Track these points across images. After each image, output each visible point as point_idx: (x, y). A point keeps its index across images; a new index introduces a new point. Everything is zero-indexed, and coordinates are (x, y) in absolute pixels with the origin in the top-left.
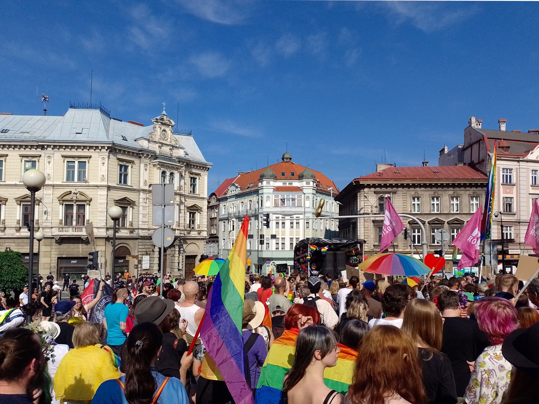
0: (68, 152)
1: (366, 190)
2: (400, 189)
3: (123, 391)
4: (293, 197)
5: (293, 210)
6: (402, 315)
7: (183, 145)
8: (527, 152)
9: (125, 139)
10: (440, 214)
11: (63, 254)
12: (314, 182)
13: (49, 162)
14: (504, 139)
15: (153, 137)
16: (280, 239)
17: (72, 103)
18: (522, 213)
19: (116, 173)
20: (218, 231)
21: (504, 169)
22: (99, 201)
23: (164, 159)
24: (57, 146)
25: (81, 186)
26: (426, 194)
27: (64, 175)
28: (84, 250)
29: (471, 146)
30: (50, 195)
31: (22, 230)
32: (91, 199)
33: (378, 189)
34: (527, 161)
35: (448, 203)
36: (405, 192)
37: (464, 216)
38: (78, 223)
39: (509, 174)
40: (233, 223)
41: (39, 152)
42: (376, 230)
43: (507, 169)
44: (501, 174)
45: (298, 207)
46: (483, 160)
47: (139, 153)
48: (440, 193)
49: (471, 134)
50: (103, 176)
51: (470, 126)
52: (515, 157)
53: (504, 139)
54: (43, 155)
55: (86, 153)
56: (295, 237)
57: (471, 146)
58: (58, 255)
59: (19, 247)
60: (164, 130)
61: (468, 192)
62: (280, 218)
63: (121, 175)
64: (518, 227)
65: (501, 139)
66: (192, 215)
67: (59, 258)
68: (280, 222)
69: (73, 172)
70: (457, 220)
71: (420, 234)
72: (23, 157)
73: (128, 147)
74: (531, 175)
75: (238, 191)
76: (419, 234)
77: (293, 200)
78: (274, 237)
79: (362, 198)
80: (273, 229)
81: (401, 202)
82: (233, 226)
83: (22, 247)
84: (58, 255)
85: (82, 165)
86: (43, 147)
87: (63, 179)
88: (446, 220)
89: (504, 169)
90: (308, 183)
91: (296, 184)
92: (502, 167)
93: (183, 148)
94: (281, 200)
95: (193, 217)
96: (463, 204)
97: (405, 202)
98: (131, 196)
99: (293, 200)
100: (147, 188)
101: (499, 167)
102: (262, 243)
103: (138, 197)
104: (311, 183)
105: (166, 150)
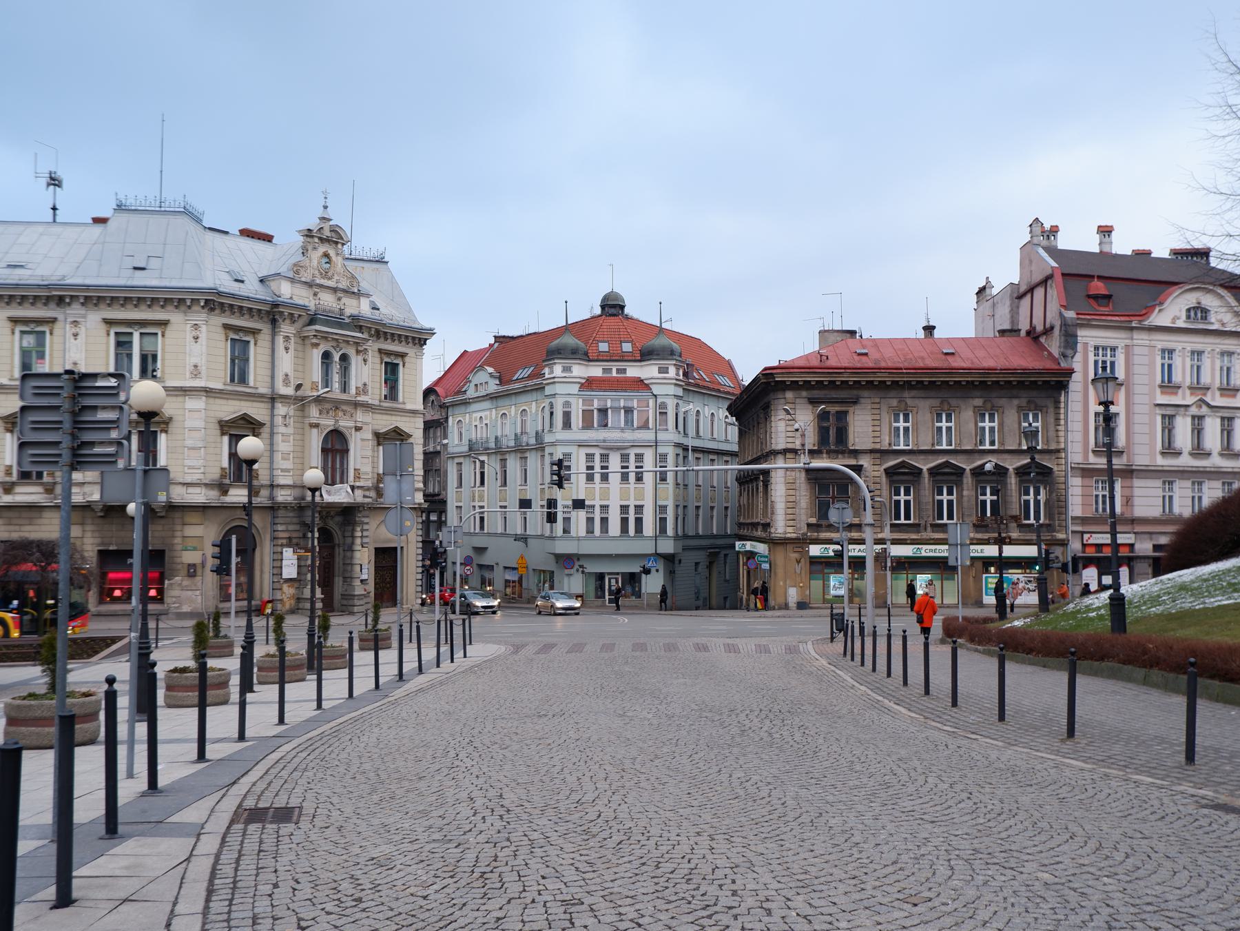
1: (789, 395)
2: (865, 393)
4: (629, 404)
5: (629, 436)
8: (1149, 310)
10: (911, 452)
11: (110, 544)
12: (677, 367)
13: (75, 335)
14: (1099, 277)
16: (597, 509)
18: (1137, 449)
19: (222, 360)
20: (444, 486)
21: (1096, 348)
22: (188, 424)
23: (327, 323)
26: (923, 408)
29: (1031, 290)
31: (232, 492)
32: (171, 419)
33: (816, 394)
35: (972, 426)
36: (877, 400)
37: (1006, 456)
39: (1108, 359)
42: (812, 489)
43: (1104, 348)
44: (1092, 358)
45: (639, 428)
47: (273, 313)
49: (1031, 261)
50: (196, 366)
52: (1123, 319)
53: (1099, 277)
54: (60, 317)
56: (632, 503)
57: (1031, 290)
58: (99, 545)
59: (12, 528)
61: (1016, 402)
62: (597, 458)
64: (1127, 483)
65: (1093, 277)
67: (102, 553)
68: (597, 469)
69: (130, 356)
71: (911, 498)
73: (248, 299)
74: (1159, 361)
75: (493, 386)
76: (907, 498)
77: (629, 411)
78: (579, 504)
79: (782, 415)
80: (578, 486)
82: (482, 474)
83: (17, 528)
84: (99, 545)
86: (60, 301)
87: (12, 371)
88: (925, 465)
89: (1096, 348)
90: (663, 370)
91: (633, 371)
92: (1092, 343)
93: (368, 296)
94: (599, 410)
96: (1006, 429)
97: (877, 423)
98: (258, 411)
99: (629, 411)
100: (289, 391)
102: (551, 518)
103: (269, 412)
104: (672, 371)
105: (328, 301)
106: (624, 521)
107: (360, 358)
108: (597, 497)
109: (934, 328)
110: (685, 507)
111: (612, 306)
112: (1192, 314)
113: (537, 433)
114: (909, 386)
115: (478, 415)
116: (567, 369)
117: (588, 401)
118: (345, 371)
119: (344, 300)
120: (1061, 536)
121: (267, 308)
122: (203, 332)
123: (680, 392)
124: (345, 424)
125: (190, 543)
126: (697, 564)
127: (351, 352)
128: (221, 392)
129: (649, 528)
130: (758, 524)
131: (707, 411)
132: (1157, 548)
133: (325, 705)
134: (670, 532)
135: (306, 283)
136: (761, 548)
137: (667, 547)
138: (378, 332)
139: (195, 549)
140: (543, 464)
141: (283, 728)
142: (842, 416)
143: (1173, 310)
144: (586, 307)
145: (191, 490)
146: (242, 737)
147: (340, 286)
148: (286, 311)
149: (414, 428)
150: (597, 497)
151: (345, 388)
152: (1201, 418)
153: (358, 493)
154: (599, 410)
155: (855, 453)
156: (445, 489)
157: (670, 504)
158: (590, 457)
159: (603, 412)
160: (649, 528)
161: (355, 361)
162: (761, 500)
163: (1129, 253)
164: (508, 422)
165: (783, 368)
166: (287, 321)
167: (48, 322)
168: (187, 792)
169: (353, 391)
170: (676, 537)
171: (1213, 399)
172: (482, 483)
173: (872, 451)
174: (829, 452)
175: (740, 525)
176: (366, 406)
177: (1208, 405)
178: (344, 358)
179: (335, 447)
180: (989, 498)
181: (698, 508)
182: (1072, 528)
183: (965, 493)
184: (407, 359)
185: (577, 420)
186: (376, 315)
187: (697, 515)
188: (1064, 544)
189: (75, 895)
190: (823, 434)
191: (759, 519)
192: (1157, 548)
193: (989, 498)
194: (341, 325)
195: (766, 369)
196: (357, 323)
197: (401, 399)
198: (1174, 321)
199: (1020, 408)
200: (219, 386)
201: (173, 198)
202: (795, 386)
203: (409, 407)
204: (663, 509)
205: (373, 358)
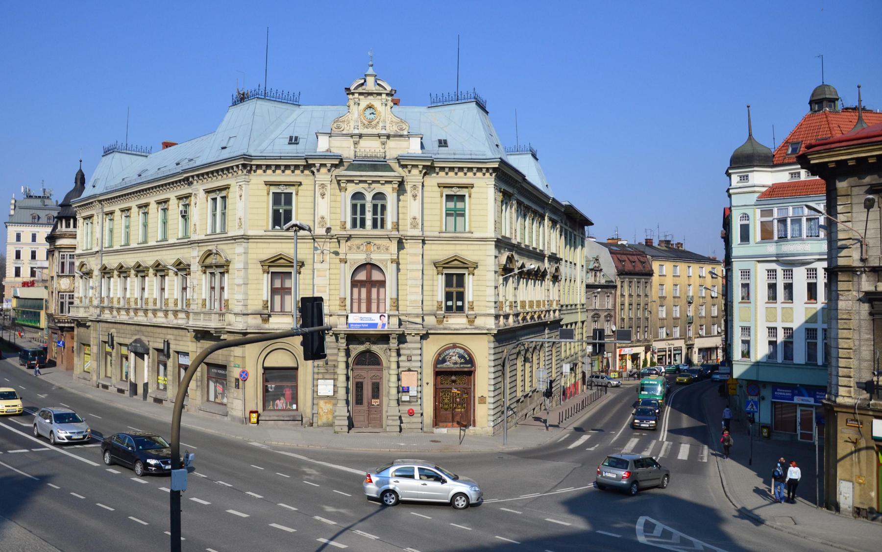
3: (799, 420)
6: (787, 480)
15: (343, 126)
32: (189, 265)
41: (297, 176)
50: (415, 218)
56: (820, 326)
60: (370, 107)
72: (271, 185)
87: (441, 227)
108: (779, 318)
116: (744, 178)
117: (764, 213)
121: (303, 163)
128: (260, 237)
148: (318, 163)
150: (779, 318)
158: (772, 273)
163: (564, 203)
185: (756, 233)
200: (262, 233)
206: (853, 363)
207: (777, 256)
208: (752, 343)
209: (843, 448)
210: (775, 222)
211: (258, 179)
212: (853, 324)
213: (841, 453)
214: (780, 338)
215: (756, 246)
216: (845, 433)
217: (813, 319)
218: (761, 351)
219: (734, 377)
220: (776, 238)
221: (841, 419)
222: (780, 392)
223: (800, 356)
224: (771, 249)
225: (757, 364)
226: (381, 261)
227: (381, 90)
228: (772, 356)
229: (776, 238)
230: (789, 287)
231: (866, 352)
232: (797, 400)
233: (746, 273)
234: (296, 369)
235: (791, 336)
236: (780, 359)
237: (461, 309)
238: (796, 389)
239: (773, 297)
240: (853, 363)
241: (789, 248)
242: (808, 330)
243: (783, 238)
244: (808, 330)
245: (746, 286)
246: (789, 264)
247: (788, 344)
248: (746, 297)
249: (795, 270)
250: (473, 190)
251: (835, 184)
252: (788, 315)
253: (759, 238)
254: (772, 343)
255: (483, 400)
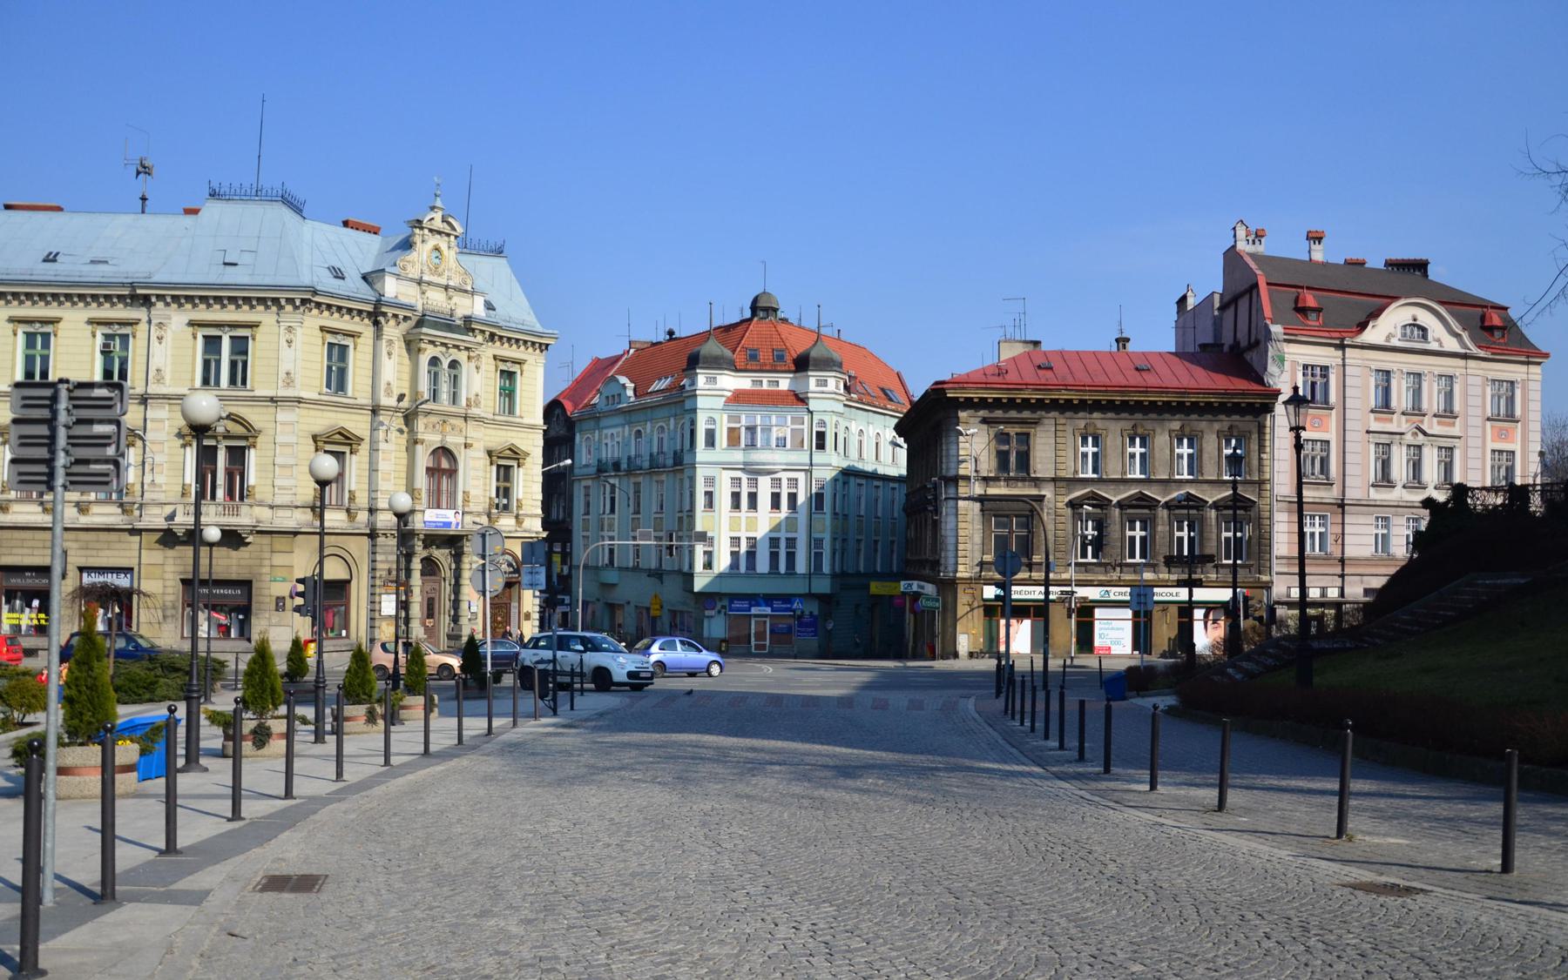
0: (203, 314)
7: (480, 284)
8: (1362, 326)
9: (338, 275)
10: (1100, 481)
17: (215, 185)
20: (569, 511)
23: (436, 325)
24: (182, 296)
25: (237, 399)
26: (1113, 429)
27: (193, 371)
28: (243, 562)
30: (162, 421)
34: (1363, 347)
37: (1205, 486)
38: (230, 493)
40: (613, 492)
46: (1257, 343)
48: (1149, 425)
51: (1234, 247)
55: (244, 315)
56: (783, 535)
59: (89, 552)
61: (1217, 426)
63: (329, 368)
66: (505, 474)
69: (218, 362)
70: (1189, 497)
81: (1055, 450)
82: (613, 500)
85: (240, 346)
86: (146, 301)
87: (193, 380)
89: (1305, 367)
93: (482, 294)
94: (748, 428)
95: (507, 478)
98: (358, 424)
100: (392, 402)
101: (1290, 363)
106: (774, 556)
107: (473, 364)
109: (1128, 340)
110: (844, 540)
111: (761, 308)
112: (1408, 330)
113: (675, 453)
114: (1097, 406)
115: (609, 432)
117: (731, 419)
118: (455, 380)
119: (455, 299)
120: (1265, 578)
122: (300, 335)
123: (839, 408)
124: (453, 441)
125: (279, 573)
126: (857, 606)
127: (462, 356)
129: (801, 566)
130: (927, 561)
131: (871, 431)
132: (1367, 592)
133: (394, 760)
134: (826, 569)
135: (412, 280)
136: (930, 589)
137: (823, 586)
138: (492, 335)
139: (284, 580)
140: (682, 488)
141: (340, 785)
142: (1025, 438)
143: (1390, 324)
144: (734, 310)
145: (281, 513)
146: (288, 794)
147: (451, 283)
148: (390, 311)
149: (533, 444)
151: (454, 399)
152: (1419, 447)
153: (468, 519)
154: (748, 428)
155: (1037, 482)
156: (570, 514)
157: (827, 538)
159: (751, 429)
160: (801, 566)
161: (466, 368)
162: (929, 533)
164: (643, 440)
165: (958, 383)
166: (392, 322)
167: (131, 324)
168: (210, 852)
169: (464, 403)
170: (834, 576)
171: (1431, 427)
172: (612, 511)
173: (1054, 480)
174: (1008, 480)
175: (907, 562)
176: (479, 420)
177: (1425, 434)
178: (454, 364)
179: (444, 465)
180: (1138, 533)
181: (859, 541)
182: (1276, 569)
183: (1160, 528)
184: (525, 367)
185: (722, 438)
186: (494, 317)
187: (859, 550)
188: (1268, 587)
189: (42, 964)
190: (1003, 458)
191: (928, 555)
192: (1367, 592)
193: (1138, 533)
194: (450, 328)
195: (937, 383)
196: (468, 325)
197: (518, 412)
198: (1388, 338)
199: (1219, 434)
200: (316, 396)
201: (270, 182)
202: (969, 404)
203: (526, 421)
204: (819, 543)
205: (488, 365)
206: (969, 546)
207: (745, 463)
208: (715, 555)
209: (962, 609)
210: (743, 430)
211: (314, 320)
212: (969, 518)
213: (960, 613)
214: (744, 548)
215: (722, 452)
216: (963, 598)
217: (777, 528)
218: (723, 562)
219: (697, 589)
220: (743, 445)
221: (960, 588)
222: (736, 605)
223: (763, 565)
224: (738, 456)
225: (721, 576)
226: (457, 445)
227: (447, 229)
228: (735, 564)
229: (743, 445)
230: (753, 497)
231: (978, 538)
232: (754, 611)
233: (710, 481)
234: (348, 582)
235: (754, 546)
236: (743, 569)
237: (506, 507)
238: (753, 599)
239: (736, 505)
240: (969, 546)
241: (758, 456)
242: (771, 539)
243: (752, 445)
244: (771, 539)
245: (709, 495)
246: (754, 472)
247: (751, 555)
248: (710, 504)
249: (760, 479)
250: (359, 341)
251: (1544, 516)
252: (752, 524)
253: (725, 444)
254: (735, 555)
255: (528, 616)
